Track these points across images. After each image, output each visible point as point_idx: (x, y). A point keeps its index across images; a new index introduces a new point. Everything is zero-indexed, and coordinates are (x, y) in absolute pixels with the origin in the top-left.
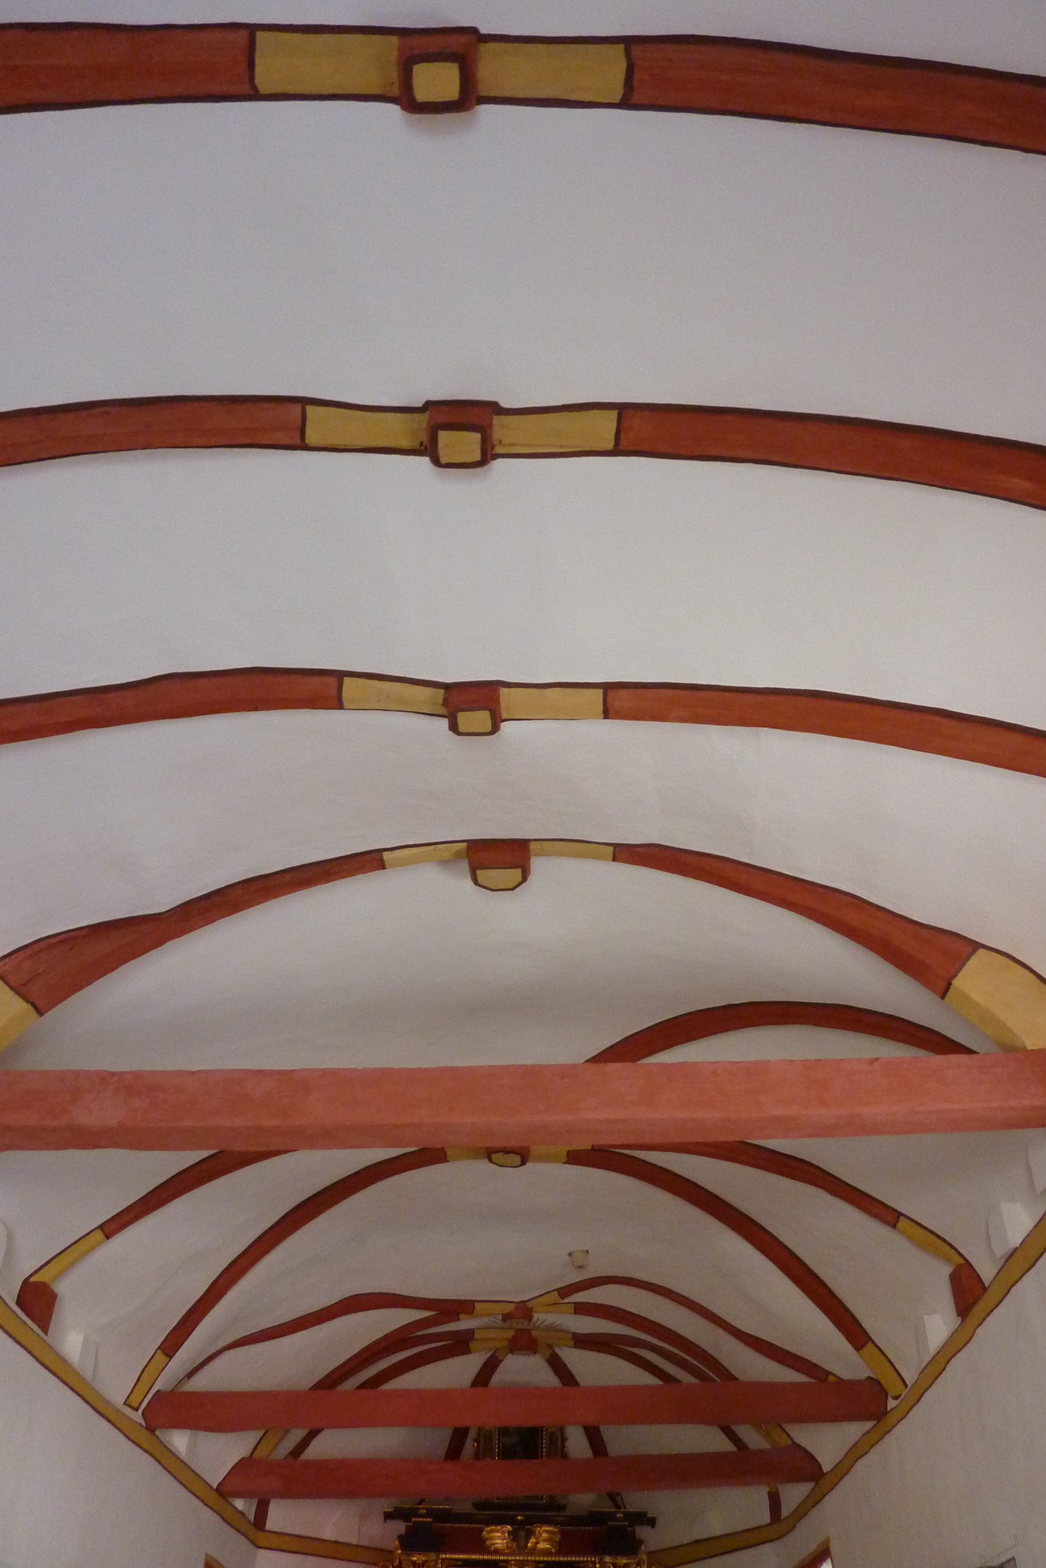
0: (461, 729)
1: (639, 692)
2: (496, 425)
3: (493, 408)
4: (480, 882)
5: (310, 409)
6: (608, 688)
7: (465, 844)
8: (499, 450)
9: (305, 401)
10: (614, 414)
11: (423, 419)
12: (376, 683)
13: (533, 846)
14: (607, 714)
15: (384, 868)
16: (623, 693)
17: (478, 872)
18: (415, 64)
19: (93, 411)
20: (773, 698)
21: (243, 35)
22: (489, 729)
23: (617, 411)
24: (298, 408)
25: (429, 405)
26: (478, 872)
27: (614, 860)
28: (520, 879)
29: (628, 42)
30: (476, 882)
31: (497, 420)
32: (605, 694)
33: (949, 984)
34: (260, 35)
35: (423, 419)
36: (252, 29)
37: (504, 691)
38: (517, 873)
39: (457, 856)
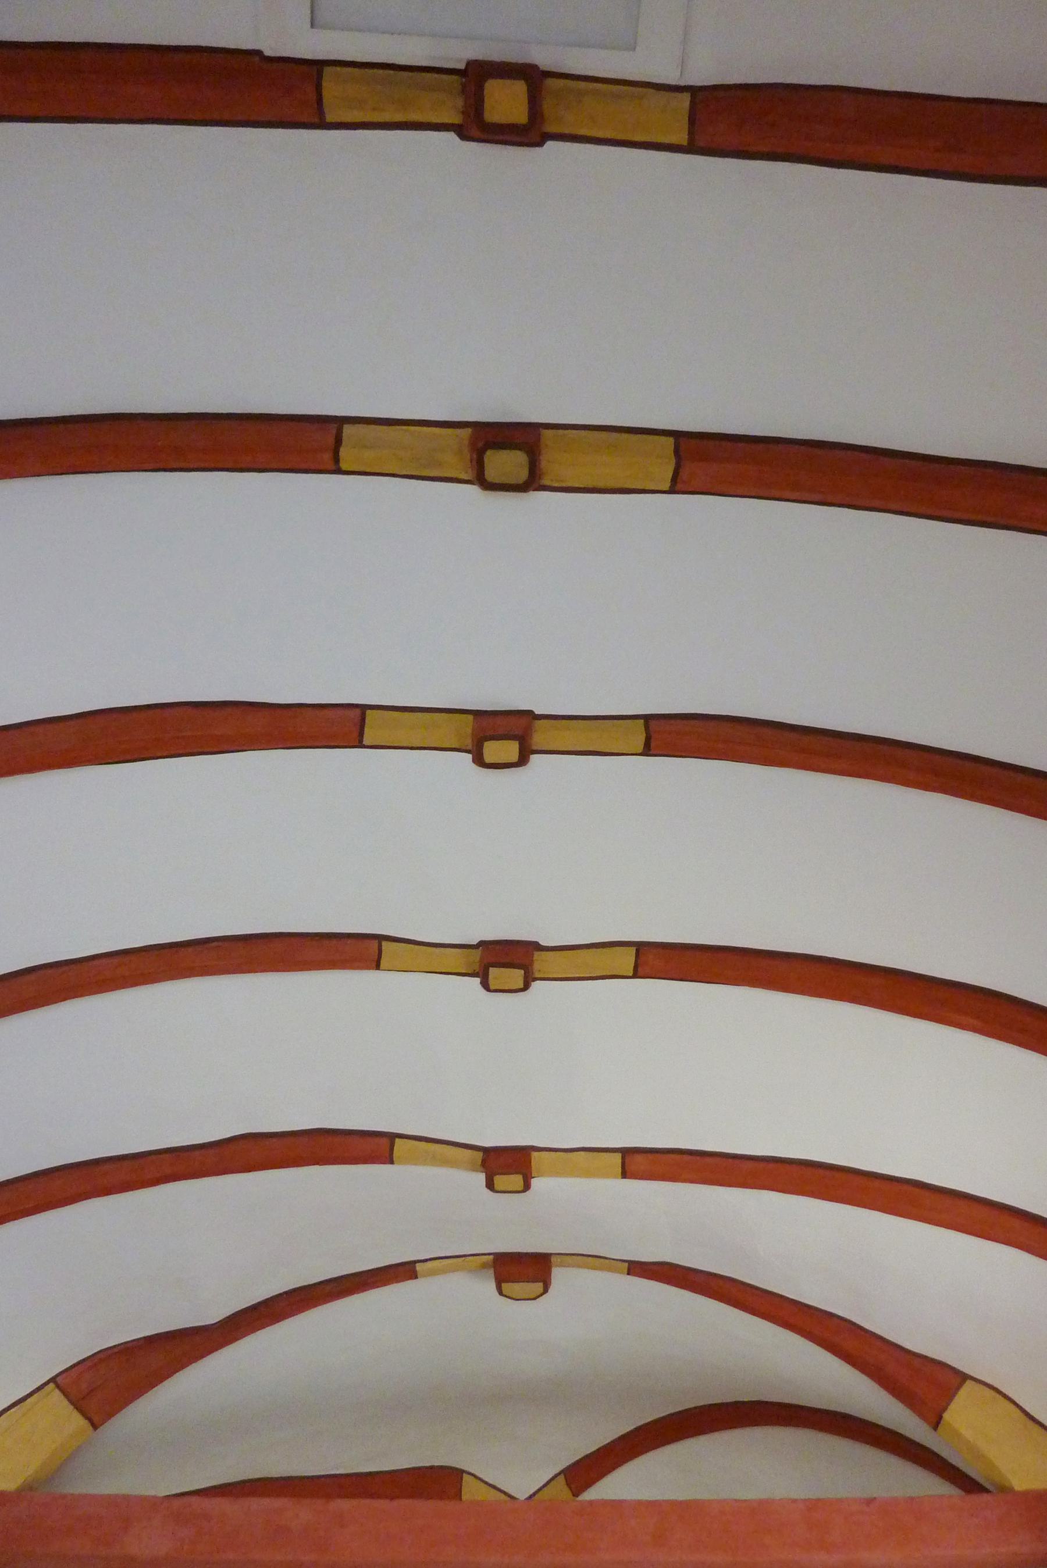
0: (492, 987)
1: (650, 1156)
2: (537, 960)
3: (536, 946)
4: (504, 1293)
5: (384, 943)
6: (627, 1153)
7: (491, 1257)
8: (537, 975)
9: (380, 938)
10: (632, 951)
11: (477, 954)
12: (423, 1144)
13: (553, 1259)
14: (625, 1175)
15: (416, 1277)
16: (639, 1158)
17: (504, 1285)
18: (486, 741)
19: (207, 945)
20: (771, 1166)
21: (358, 711)
22: (521, 986)
23: (635, 948)
24: (375, 943)
25: (482, 944)
26: (504, 1285)
27: (628, 1274)
28: (541, 1290)
29: (647, 718)
30: (501, 1293)
31: (537, 955)
32: (623, 1158)
33: (940, 1418)
34: (369, 712)
35: (477, 954)
36: (363, 708)
37: (535, 1155)
38: (539, 1287)
39: (484, 1266)
